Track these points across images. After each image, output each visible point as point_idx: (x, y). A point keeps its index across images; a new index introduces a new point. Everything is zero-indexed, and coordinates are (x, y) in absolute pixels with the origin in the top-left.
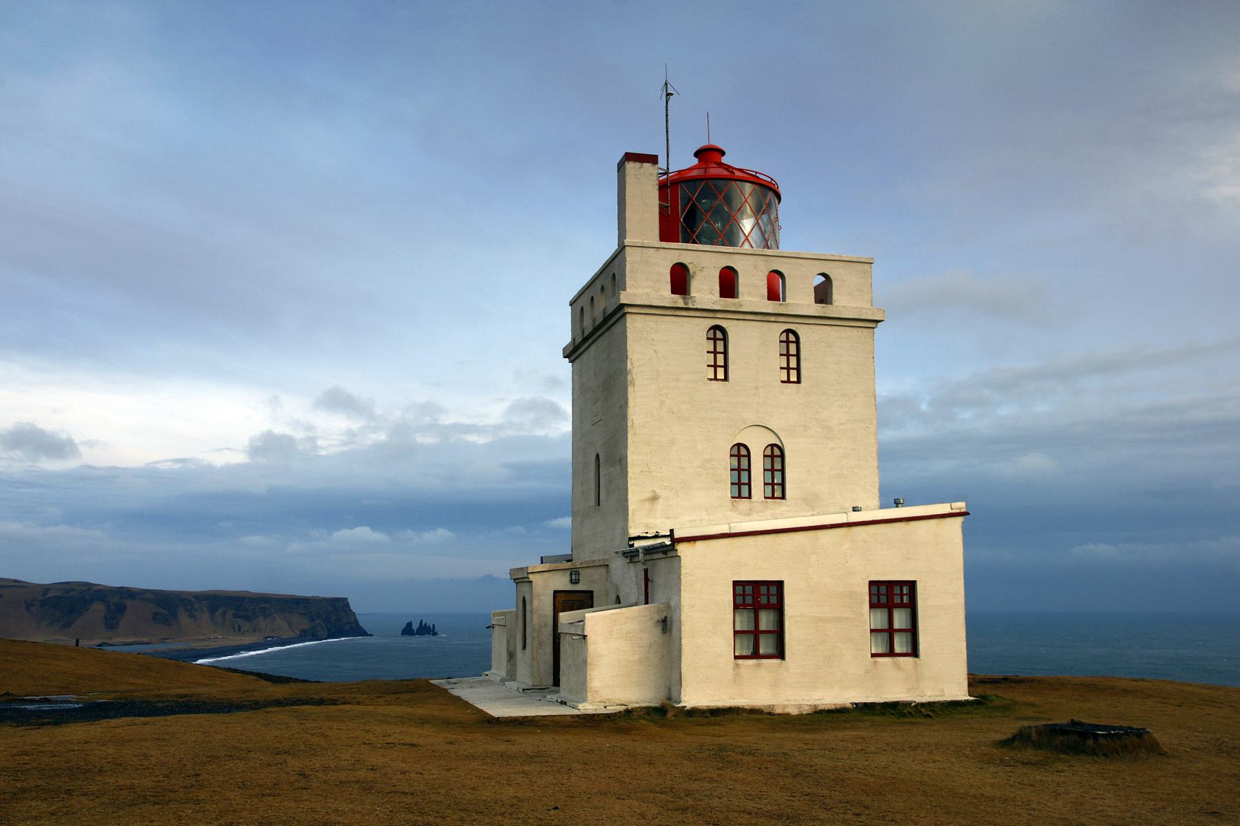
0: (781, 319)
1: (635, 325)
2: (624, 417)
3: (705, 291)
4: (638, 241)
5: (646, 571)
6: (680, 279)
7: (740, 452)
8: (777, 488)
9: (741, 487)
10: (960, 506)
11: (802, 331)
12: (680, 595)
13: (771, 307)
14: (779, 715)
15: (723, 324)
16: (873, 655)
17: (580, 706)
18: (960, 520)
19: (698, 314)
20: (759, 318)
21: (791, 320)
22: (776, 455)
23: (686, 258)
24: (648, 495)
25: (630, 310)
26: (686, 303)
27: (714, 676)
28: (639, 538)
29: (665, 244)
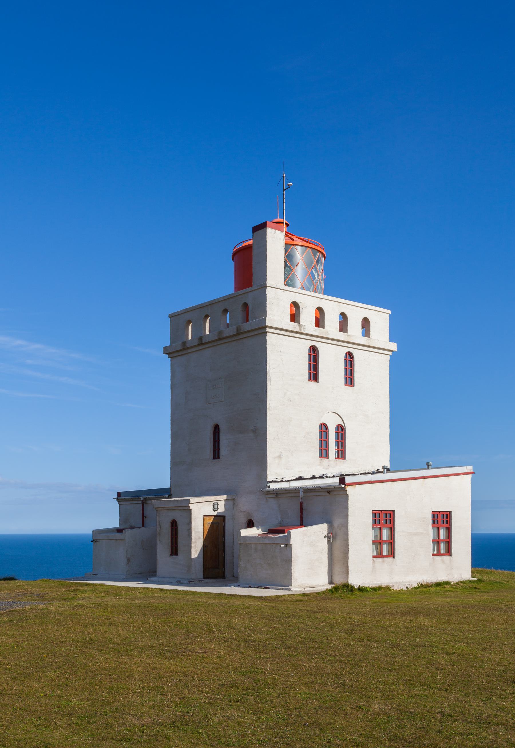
1: (272, 340)
3: (308, 318)
5: (301, 503)
7: (324, 427)
8: (341, 454)
9: (324, 453)
10: (470, 468)
13: (341, 336)
15: (317, 344)
16: (374, 557)
17: (290, 590)
18: (470, 476)
19: (305, 337)
20: (336, 343)
22: (341, 430)
23: (298, 299)
24: (277, 454)
26: (300, 330)
28: (273, 482)
29: (287, 288)
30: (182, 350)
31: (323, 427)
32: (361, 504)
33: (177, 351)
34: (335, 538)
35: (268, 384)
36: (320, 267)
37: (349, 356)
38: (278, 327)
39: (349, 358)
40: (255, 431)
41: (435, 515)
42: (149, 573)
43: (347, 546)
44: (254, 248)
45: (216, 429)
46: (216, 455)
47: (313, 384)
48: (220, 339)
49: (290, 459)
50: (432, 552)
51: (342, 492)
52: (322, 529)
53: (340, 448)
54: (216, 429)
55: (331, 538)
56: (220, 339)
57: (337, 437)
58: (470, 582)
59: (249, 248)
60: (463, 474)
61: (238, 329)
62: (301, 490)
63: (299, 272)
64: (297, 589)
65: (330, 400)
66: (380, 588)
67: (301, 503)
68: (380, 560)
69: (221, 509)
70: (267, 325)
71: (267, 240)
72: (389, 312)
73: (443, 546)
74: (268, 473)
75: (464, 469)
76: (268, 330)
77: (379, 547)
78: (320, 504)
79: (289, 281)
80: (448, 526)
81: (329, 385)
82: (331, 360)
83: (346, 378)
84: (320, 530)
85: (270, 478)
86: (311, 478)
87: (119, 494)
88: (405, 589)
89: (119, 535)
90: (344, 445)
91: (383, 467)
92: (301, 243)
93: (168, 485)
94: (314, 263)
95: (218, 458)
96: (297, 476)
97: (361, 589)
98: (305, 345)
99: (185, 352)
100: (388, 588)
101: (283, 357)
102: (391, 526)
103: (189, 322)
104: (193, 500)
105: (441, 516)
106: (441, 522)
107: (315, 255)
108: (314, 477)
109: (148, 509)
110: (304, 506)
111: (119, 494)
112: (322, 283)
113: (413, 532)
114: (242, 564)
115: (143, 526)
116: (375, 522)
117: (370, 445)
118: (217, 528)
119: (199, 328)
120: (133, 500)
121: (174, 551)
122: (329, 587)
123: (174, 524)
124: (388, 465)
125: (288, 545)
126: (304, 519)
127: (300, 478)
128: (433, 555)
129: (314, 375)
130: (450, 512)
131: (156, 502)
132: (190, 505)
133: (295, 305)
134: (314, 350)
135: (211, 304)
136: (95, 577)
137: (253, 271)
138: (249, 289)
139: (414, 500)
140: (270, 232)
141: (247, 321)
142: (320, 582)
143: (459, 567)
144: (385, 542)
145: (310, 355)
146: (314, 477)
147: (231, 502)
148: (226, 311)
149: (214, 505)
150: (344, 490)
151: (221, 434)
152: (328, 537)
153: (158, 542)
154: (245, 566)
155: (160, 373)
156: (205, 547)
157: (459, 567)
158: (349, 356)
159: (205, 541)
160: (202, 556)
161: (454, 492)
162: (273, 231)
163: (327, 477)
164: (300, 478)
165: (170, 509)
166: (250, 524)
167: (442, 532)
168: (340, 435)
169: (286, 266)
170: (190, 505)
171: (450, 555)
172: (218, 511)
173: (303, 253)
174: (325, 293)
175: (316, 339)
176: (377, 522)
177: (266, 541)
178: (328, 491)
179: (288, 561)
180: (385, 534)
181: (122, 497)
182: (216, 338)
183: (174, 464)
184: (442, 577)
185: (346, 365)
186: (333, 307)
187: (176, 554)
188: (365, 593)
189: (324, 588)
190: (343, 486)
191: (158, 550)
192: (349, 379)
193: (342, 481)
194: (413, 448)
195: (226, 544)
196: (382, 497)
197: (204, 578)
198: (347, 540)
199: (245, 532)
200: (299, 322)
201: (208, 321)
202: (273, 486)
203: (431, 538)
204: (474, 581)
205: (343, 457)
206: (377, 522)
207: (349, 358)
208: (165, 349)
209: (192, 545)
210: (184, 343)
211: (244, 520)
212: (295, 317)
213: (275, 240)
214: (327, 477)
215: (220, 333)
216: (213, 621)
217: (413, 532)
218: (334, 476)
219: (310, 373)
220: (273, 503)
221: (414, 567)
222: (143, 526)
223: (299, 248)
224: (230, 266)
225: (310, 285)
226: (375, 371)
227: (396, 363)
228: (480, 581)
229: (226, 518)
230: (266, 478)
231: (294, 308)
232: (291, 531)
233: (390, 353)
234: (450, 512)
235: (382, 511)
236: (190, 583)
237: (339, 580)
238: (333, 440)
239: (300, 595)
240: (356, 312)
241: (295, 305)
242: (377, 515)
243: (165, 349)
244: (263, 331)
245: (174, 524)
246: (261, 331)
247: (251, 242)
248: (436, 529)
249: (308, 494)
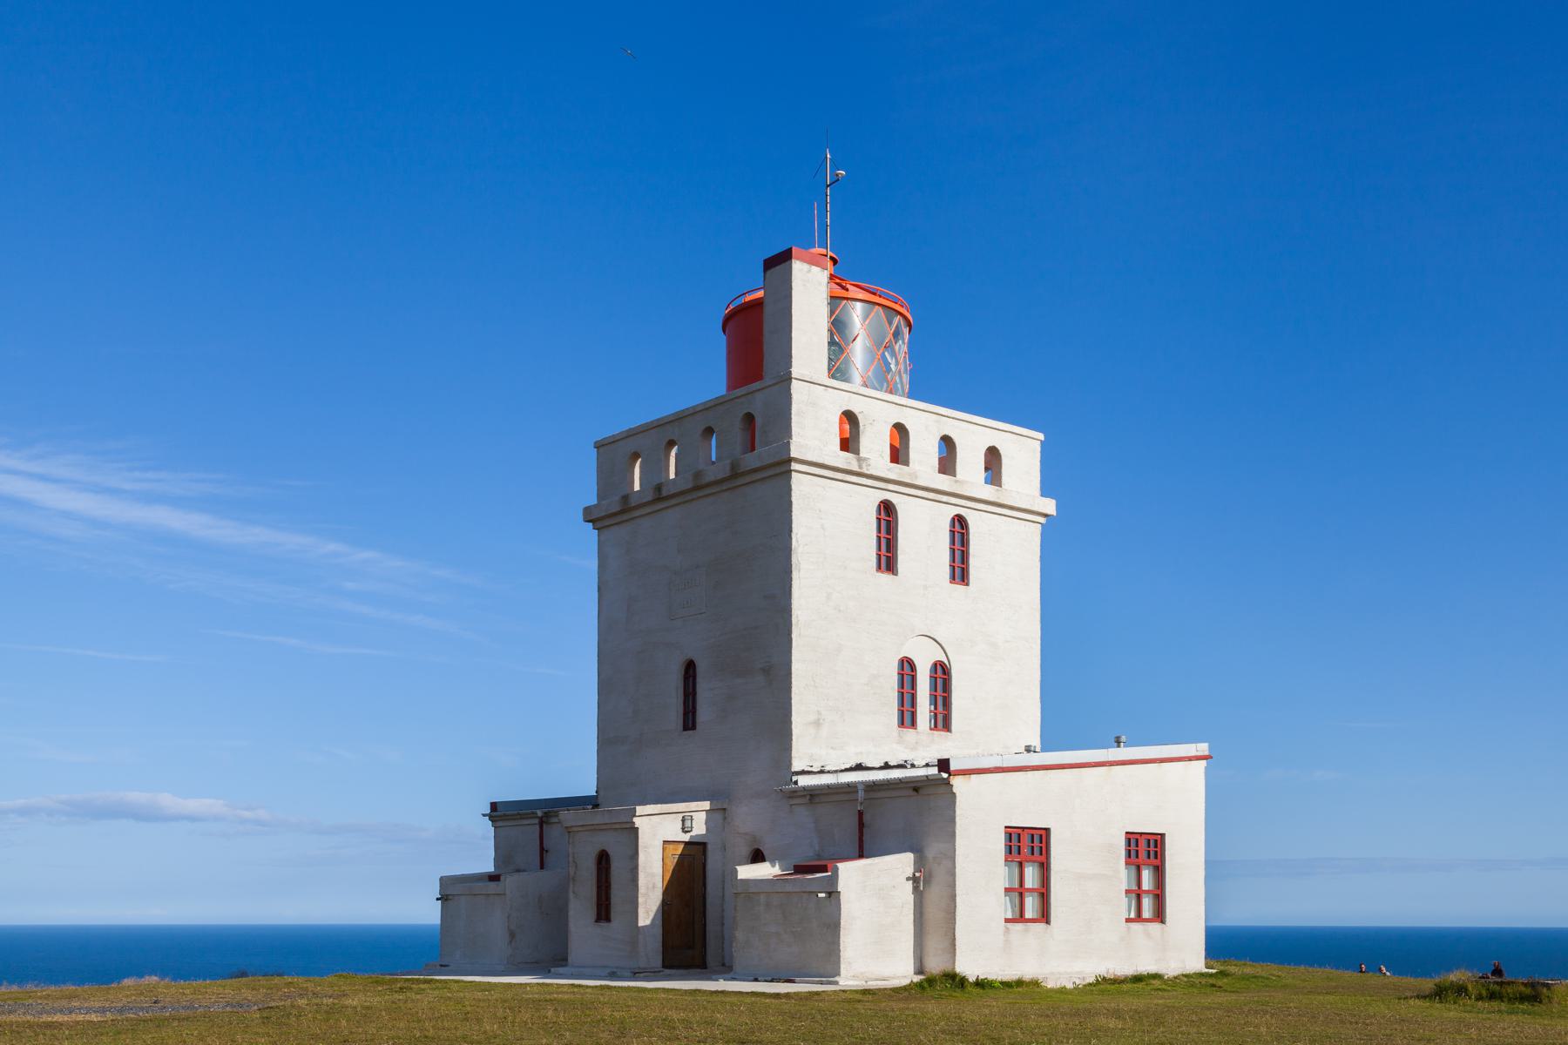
0: (953, 500)
1: (802, 486)
3: (875, 444)
4: (807, 375)
5: (861, 814)
7: (907, 667)
8: (943, 721)
9: (907, 718)
10: (1203, 748)
11: (972, 518)
12: (952, 836)
13: (943, 482)
14: (1052, 990)
16: (1007, 920)
17: (836, 983)
22: (942, 674)
24: (813, 717)
27: (987, 947)
28: (803, 772)
30: (622, 512)
31: (907, 669)
32: (980, 819)
33: (613, 514)
34: (927, 881)
35: (795, 575)
36: (901, 347)
37: (959, 524)
38: (814, 459)
39: (960, 527)
40: (767, 671)
41: (1132, 839)
42: (553, 958)
43: (953, 897)
44: (766, 302)
45: (690, 669)
46: (689, 721)
47: (886, 577)
48: (697, 487)
49: (838, 728)
51: (942, 789)
53: (940, 708)
54: (690, 669)
55: (920, 883)
56: (697, 488)
57: (934, 687)
58: (1202, 975)
59: (758, 304)
60: (1190, 759)
61: (734, 466)
62: (860, 787)
63: (858, 352)
64: (851, 983)
66: (1020, 983)
67: (861, 814)
68: (1019, 926)
69: (699, 828)
71: (794, 285)
72: (1041, 436)
73: (1150, 903)
74: (794, 753)
76: (794, 466)
77: (1016, 871)
78: (895, 814)
79: (838, 369)
80: (1157, 862)
81: (922, 572)
82: (924, 531)
83: (953, 568)
84: (901, 864)
85: (797, 765)
86: (881, 768)
87: (494, 806)
88: (1070, 986)
89: (492, 884)
90: (947, 703)
92: (861, 295)
93: (591, 790)
94: (890, 337)
95: (694, 727)
96: (852, 763)
97: (981, 984)
98: (871, 499)
99: (625, 517)
100: (1035, 983)
101: (825, 522)
102: (1043, 859)
103: (636, 456)
104: (640, 810)
105: (1143, 843)
106: (1143, 855)
107: (890, 323)
108: (886, 766)
109: (554, 834)
110: (866, 818)
111: (494, 806)
112: (906, 378)
113: (1088, 872)
114: (740, 935)
115: (542, 867)
116: (1009, 850)
117: (1001, 704)
118: (691, 867)
119: (655, 467)
120: (522, 817)
121: (603, 912)
122: (917, 979)
123: (603, 860)
125: (833, 894)
126: (866, 846)
127: (859, 767)
128: (1128, 920)
129: (888, 561)
130: (1162, 835)
131: (567, 816)
132: (635, 820)
133: (850, 417)
134: (887, 510)
135: (679, 418)
136: (444, 968)
137: (765, 347)
138: (757, 385)
139: (1091, 808)
140: (799, 268)
141: (753, 449)
142: (898, 969)
145: (879, 520)
146: (886, 766)
147: (719, 815)
148: (709, 431)
149: (683, 820)
150: (947, 783)
151: (699, 680)
152: (915, 879)
153: (571, 895)
154: (744, 941)
155: (579, 557)
156: (664, 903)
157: (1178, 949)
158: (959, 524)
159: (665, 893)
160: (659, 922)
161: (1169, 792)
162: (805, 266)
163: (913, 766)
164: (859, 767)
165: (595, 829)
166: (757, 857)
167: (1147, 876)
168: (940, 682)
169: (832, 343)
170: (635, 820)
171: (1163, 922)
172: (693, 833)
173: (866, 317)
174: (911, 396)
175: (891, 487)
176: (1015, 850)
177: (789, 888)
178: (916, 787)
179: (833, 927)
180: (1031, 876)
181: (499, 813)
182: (690, 486)
183: (607, 741)
184: (1146, 966)
185: (953, 542)
186: (927, 424)
187: (608, 920)
188: (990, 992)
189: (906, 982)
190: (945, 775)
191: (571, 913)
192: (958, 571)
195: (710, 866)
196: (1027, 802)
197: (665, 966)
199: (747, 872)
200: (856, 452)
201: (673, 453)
202: (804, 781)
203: (1125, 887)
204: (1211, 975)
205: (947, 726)
206: (1015, 850)
207: (960, 527)
208: (587, 510)
209: (641, 900)
210: (625, 498)
211: (745, 851)
212: (848, 444)
213: (809, 285)
214: (913, 766)
215: (698, 475)
216: (674, 1015)
217: (1088, 872)
218: (927, 765)
219: (879, 556)
220: (803, 814)
221: (1085, 943)
222: (542, 867)
223: (859, 305)
224: (718, 344)
225: (881, 379)
226: (1011, 553)
227: (1053, 534)
228: (1222, 974)
229: (709, 847)
230: (790, 764)
231: (847, 427)
232: (840, 865)
233: (1043, 520)
234: (1162, 835)
235: (1023, 828)
236: (635, 975)
237: (935, 966)
238: (926, 692)
239: (856, 992)
240: (974, 434)
241: (850, 417)
242: (1015, 838)
243: (587, 510)
244: (783, 469)
245: (603, 860)
246: (781, 467)
247: (760, 294)
248: (1133, 868)
249: (873, 795)
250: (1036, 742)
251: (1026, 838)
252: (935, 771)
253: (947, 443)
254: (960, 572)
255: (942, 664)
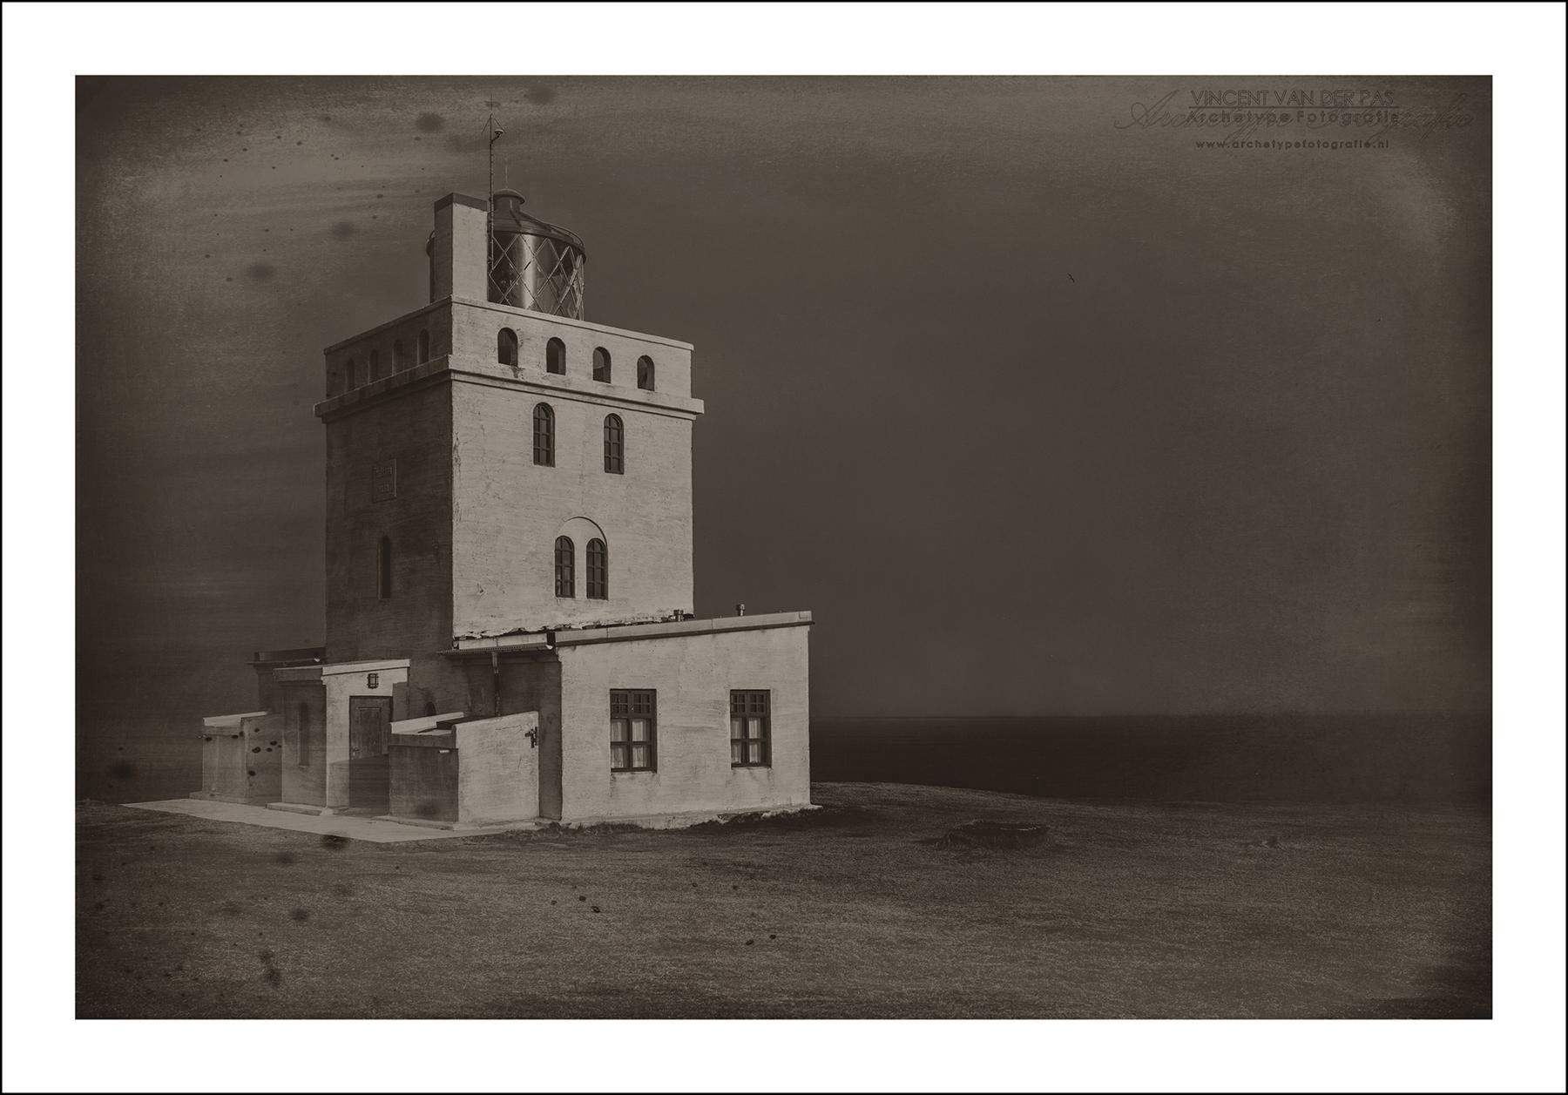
0: (607, 402)
1: (462, 394)
2: (448, 500)
3: (532, 362)
4: (467, 297)
6: (508, 346)
8: (598, 589)
9: (565, 588)
11: (626, 417)
13: (598, 388)
15: (551, 402)
18: (807, 628)
19: (526, 388)
20: (586, 398)
21: (616, 404)
22: (598, 550)
23: (515, 324)
24: (473, 590)
25: (457, 377)
27: (594, 790)
29: (536, 314)
32: (588, 678)
39: (614, 426)
41: (737, 696)
46: (387, 593)
49: (496, 597)
50: (730, 761)
52: (530, 720)
65: (577, 495)
70: (452, 366)
72: (691, 347)
73: (753, 750)
75: (795, 616)
78: (517, 677)
82: (578, 428)
85: (458, 631)
91: (676, 613)
101: (485, 425)
104: (326, 670)
113: (693, 729)
124: (688, 608)
127: (520, 632)
129: (544, 452)
140: (458, 210)
142: (521, 809)
143: (786, 786)
144: (638, 744)
150: (553, 654)
157: (786, 786)
161: (778, 655)
162: (466, 209)
180: (754, 729)
186: (581, 339)
193: (551, 639)
194: (730, 580)
198: (560, 742)
200: (515, 364)
202: (464, 646)
205: (603, 594)
207: (614, 426)
217: (693, 729)
225: (556, 301)
226: (664, 450)
233: (693, 417)
238: (582, 567)
240: (626, 347)
246: (442, 380)
250: (688, 608)
251: (631, 699)
252: (542, 639)
253: (603, 355)
254: (614, 461)
255: (599, 541)
